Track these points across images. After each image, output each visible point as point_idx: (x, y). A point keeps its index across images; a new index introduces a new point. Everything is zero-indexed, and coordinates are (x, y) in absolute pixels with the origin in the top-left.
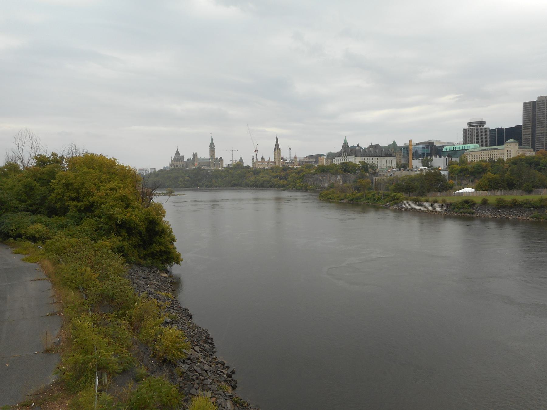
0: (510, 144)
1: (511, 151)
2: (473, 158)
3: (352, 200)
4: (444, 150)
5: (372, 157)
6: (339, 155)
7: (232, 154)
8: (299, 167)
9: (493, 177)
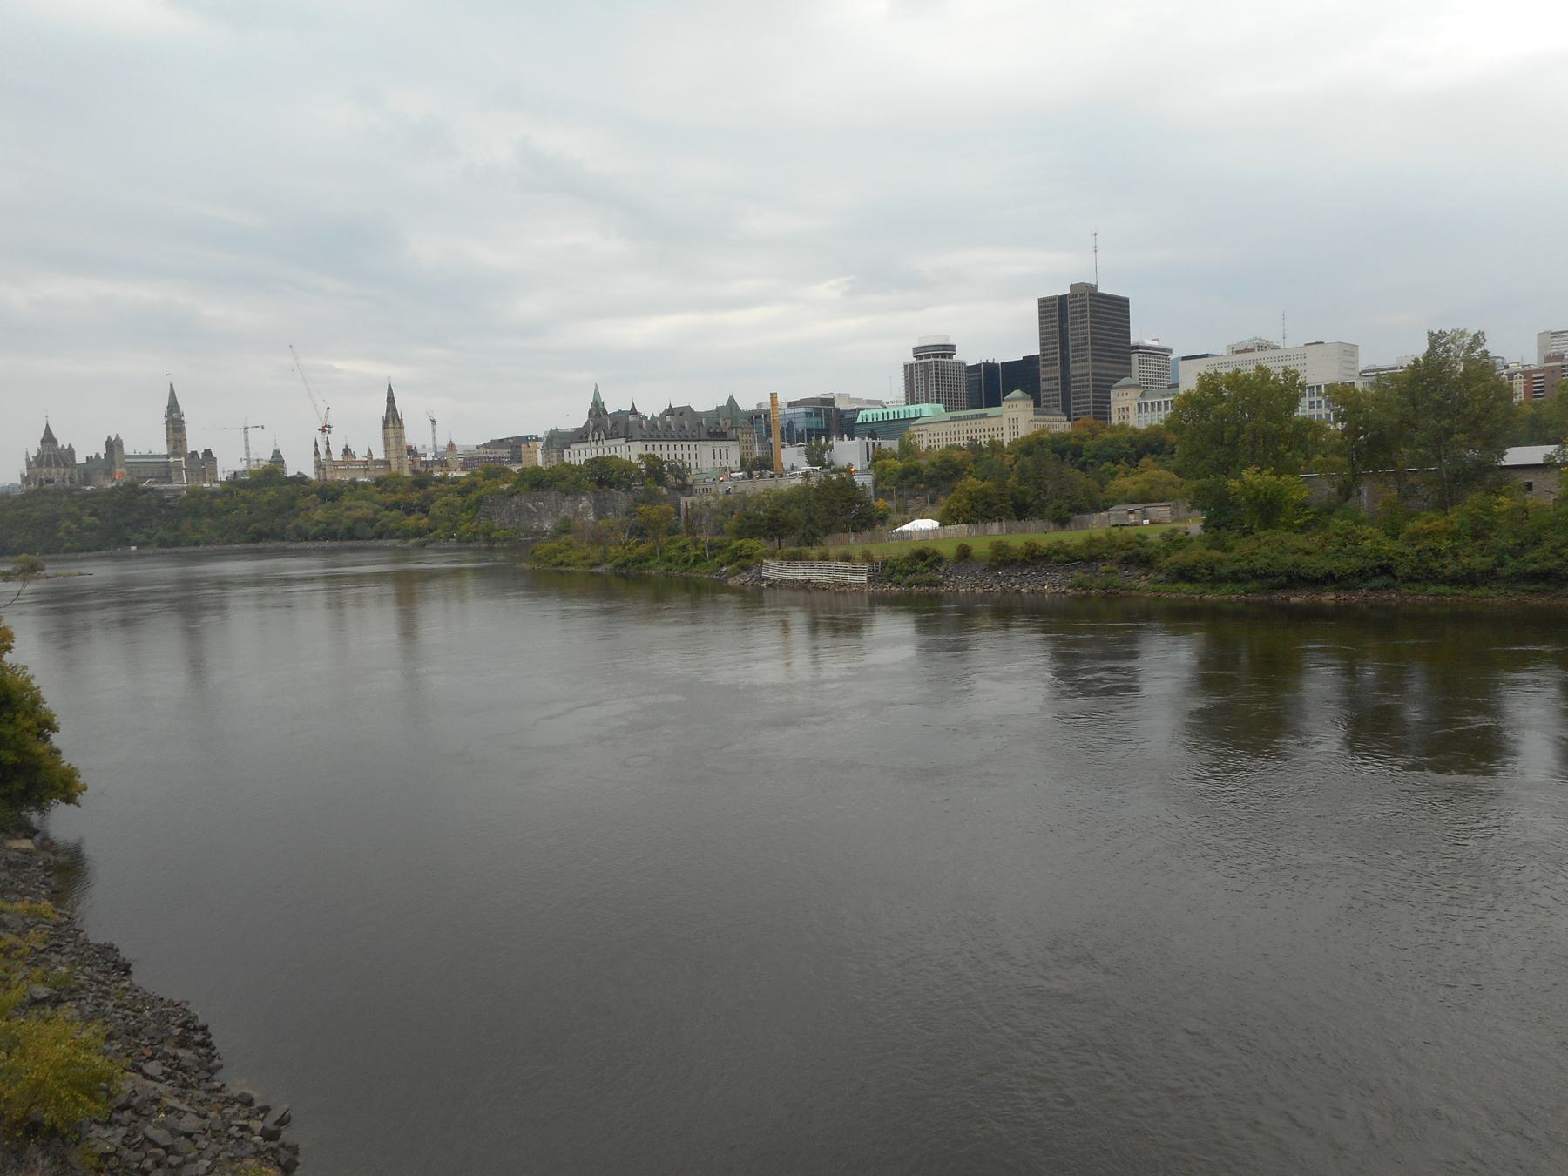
3: (625, 565)
4: (859, 421)
5: (674, 443)
6: (581, 438)
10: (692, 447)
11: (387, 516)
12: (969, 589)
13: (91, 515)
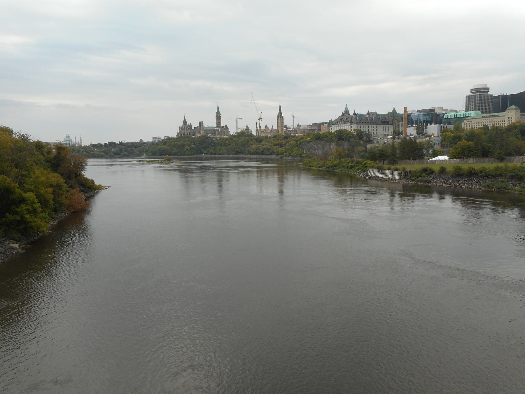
0: (511, 111)
1: (512, 118)
2: (473, 126)
3: (329, 168)
4: (445, 118)
5: (368, 125)
6: (336, 123)
7: (237, 123)
8: (301, 135)
9: (467, 144)
10: (365, 126)
11: (274, 148)
12: (441, 185)
13: (193, 144)
